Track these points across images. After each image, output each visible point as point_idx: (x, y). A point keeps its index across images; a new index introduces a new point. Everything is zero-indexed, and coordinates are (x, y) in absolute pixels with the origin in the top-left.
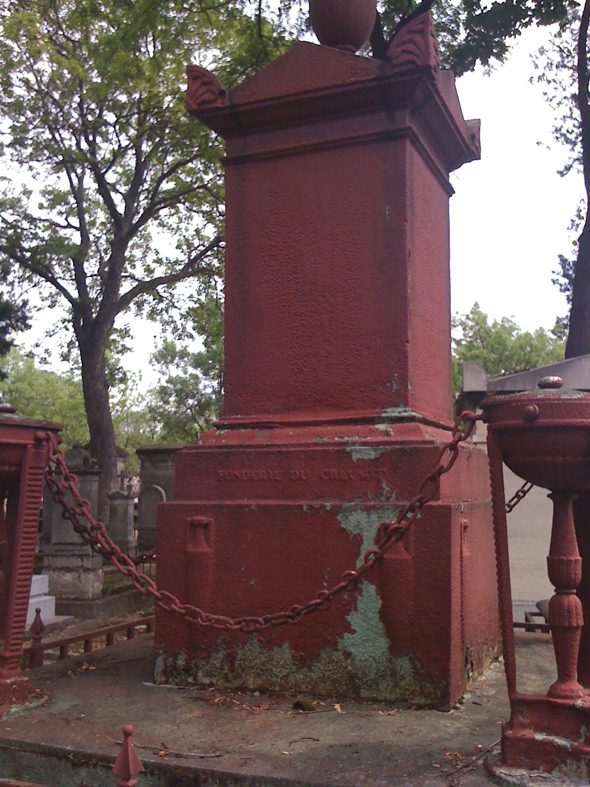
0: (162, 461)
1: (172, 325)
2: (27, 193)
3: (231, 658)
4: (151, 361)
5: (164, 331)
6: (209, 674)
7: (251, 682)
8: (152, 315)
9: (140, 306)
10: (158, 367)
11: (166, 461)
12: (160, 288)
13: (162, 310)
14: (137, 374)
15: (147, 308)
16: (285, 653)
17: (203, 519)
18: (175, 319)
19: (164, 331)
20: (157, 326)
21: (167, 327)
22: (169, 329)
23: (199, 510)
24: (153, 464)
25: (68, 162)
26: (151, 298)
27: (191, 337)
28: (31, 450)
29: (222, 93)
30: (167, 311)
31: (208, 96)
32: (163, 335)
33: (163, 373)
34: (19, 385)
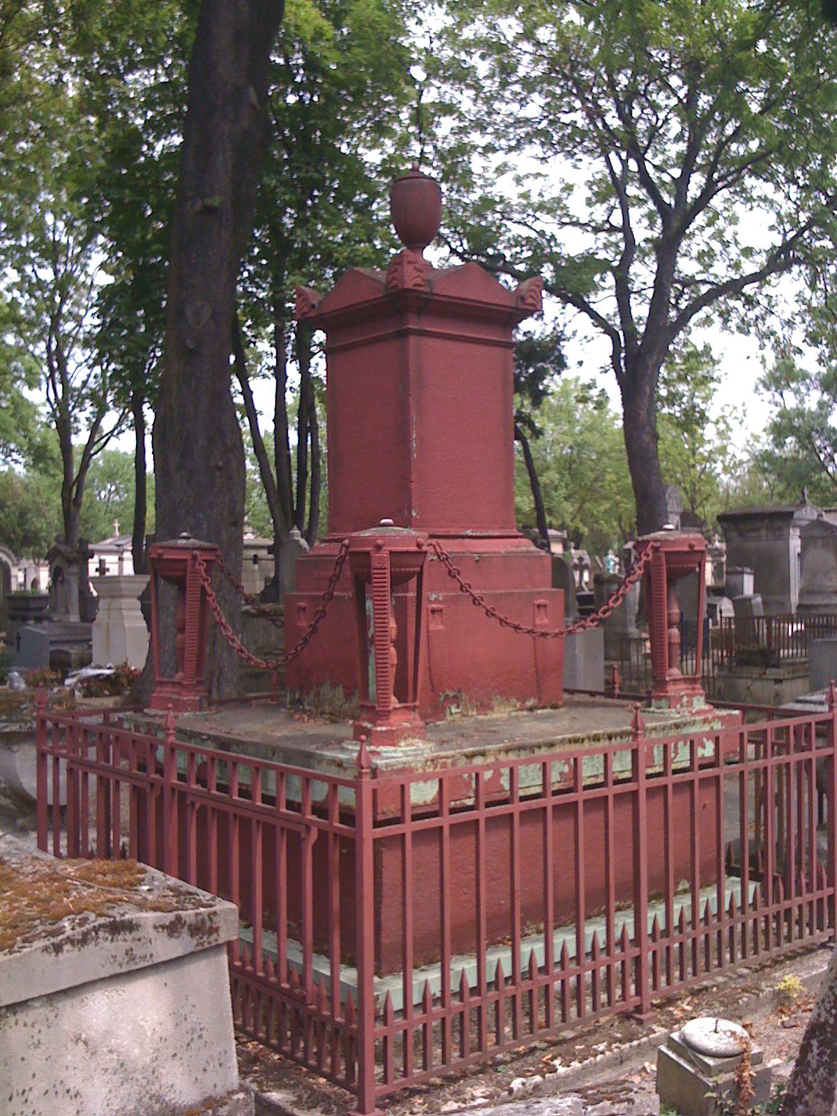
0: (753, 530)
1: (772, 338)
2: (569, 188)
3: (318, 694)
4: (757, 389)
5: (762, 347)
6: (309, 704)
7: (327, 709)
8: (744, 328)
9: (725, 315)
10: (768, 395)
11: (758, 530)
12: (749, 289)
13: (757, 318)
14: (740, 409)
15: (734, 322)
16: (340, 691)
17: (302, 604)
18: (775, 329)
19: (762, 347)
20: (752, 341)
21: (766, 341)
22: (769, 344)
23: (302, 598)
24: (741, 534)
25: (605, 143)
26: (738, 304)
27: (800, 352)
28: (190, 562)
29: (313, 306)
30: (763, 319)
31: (305, 309)
32: (761, 353)
33: (776, 404)
34: (588, 436)
